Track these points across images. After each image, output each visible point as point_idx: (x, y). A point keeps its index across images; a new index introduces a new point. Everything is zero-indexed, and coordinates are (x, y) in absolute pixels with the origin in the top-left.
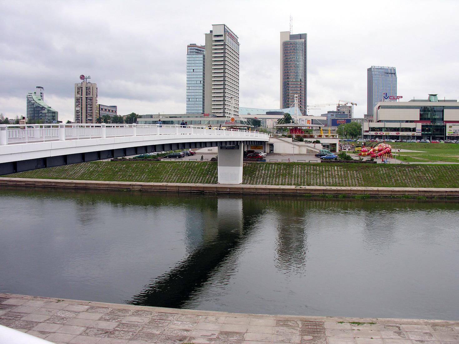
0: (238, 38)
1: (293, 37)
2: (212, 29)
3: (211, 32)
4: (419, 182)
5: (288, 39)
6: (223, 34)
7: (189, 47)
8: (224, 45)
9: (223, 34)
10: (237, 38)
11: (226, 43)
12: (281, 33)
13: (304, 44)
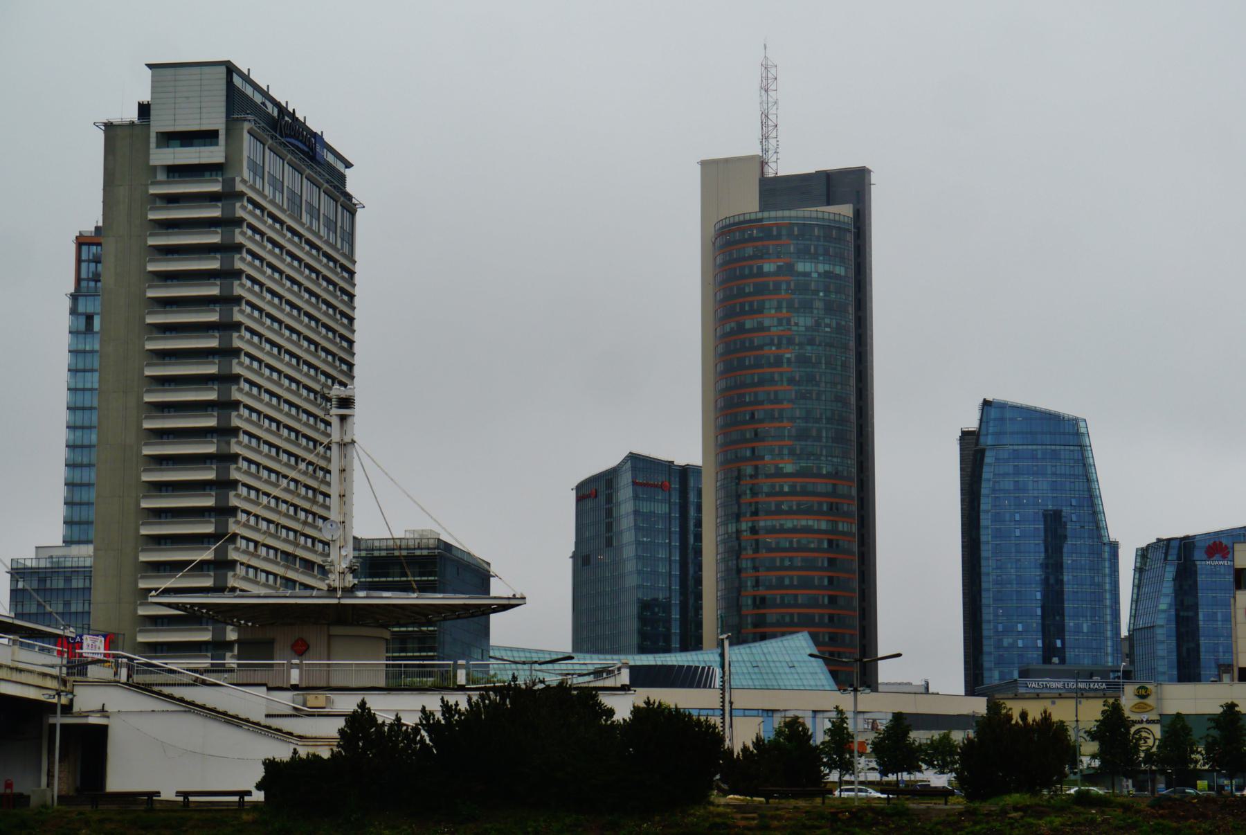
0: (348, 165)
1: (778, 190)
2: (146, 97)
3: (144, 109)
4: (54, 762)
5: (747, 203)
6: (215, 119)
7: (84, 248)
8: (229, 196)
9: (215, 119)
10: (340, 166)
11: (240, 187)
12: (708, 166)
13: (850, 237)
